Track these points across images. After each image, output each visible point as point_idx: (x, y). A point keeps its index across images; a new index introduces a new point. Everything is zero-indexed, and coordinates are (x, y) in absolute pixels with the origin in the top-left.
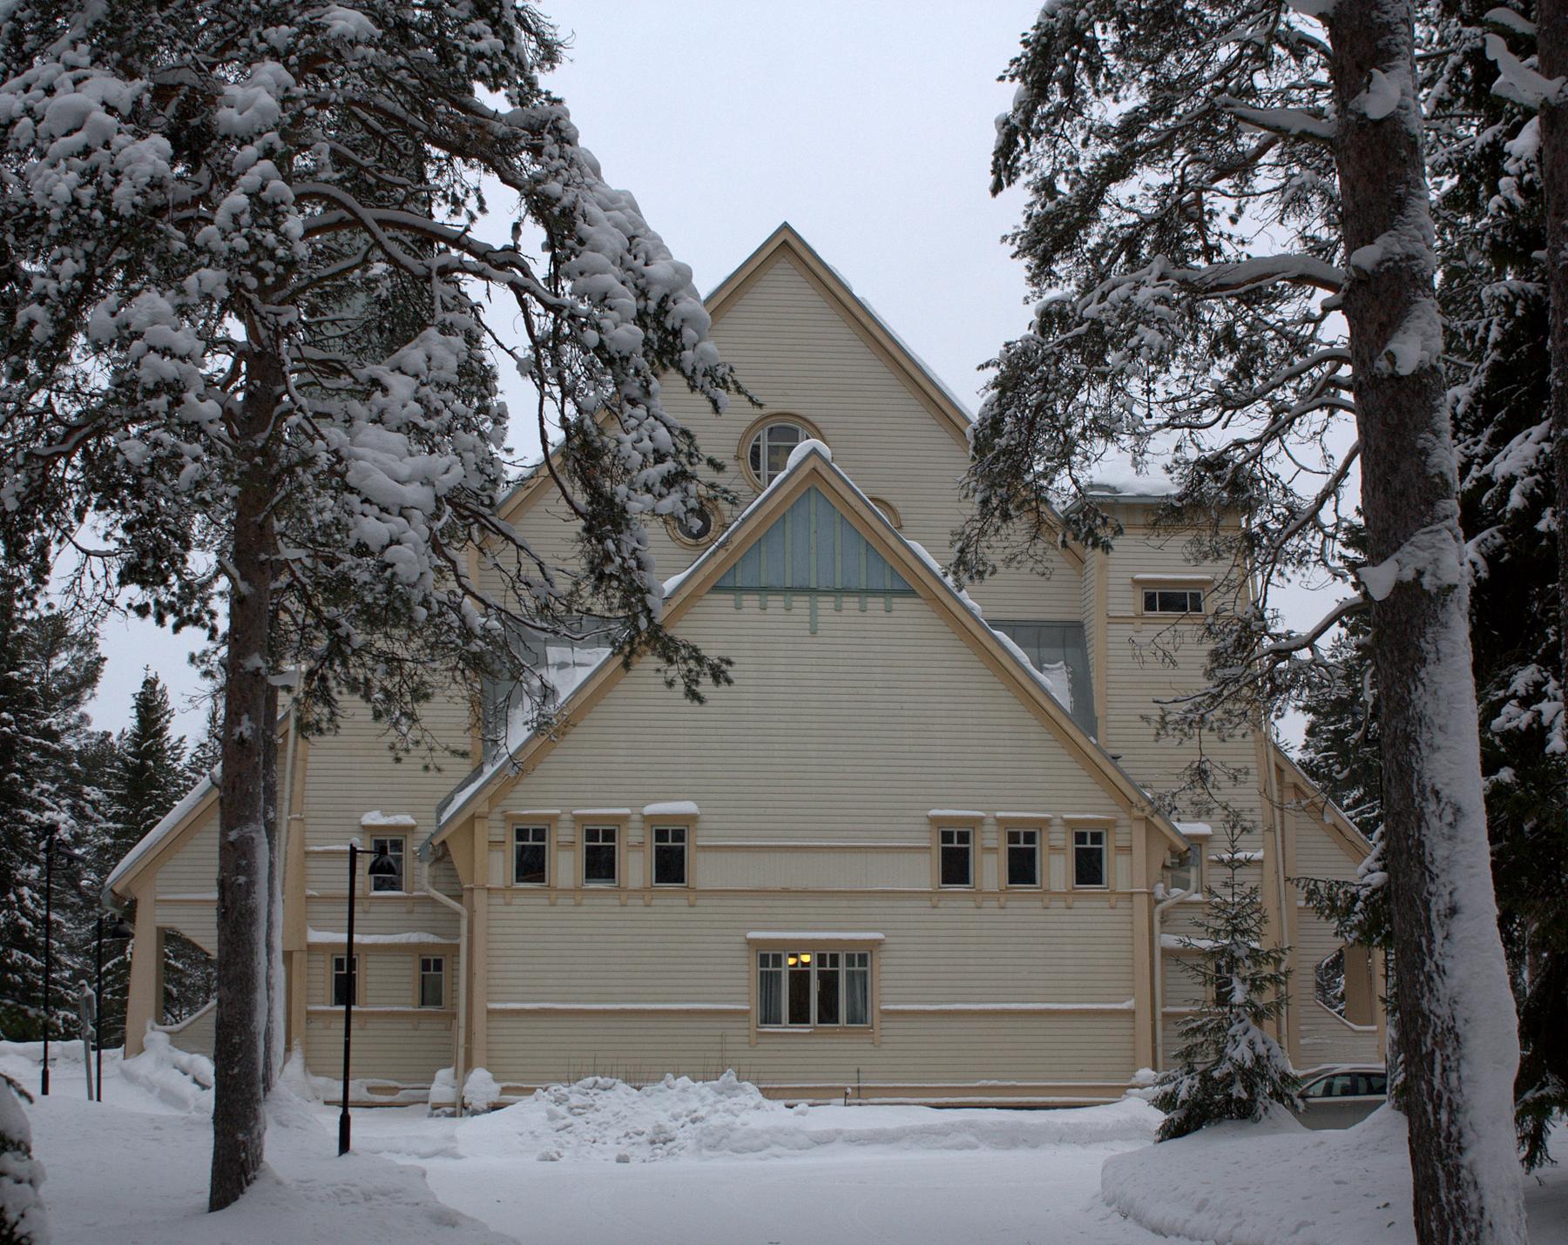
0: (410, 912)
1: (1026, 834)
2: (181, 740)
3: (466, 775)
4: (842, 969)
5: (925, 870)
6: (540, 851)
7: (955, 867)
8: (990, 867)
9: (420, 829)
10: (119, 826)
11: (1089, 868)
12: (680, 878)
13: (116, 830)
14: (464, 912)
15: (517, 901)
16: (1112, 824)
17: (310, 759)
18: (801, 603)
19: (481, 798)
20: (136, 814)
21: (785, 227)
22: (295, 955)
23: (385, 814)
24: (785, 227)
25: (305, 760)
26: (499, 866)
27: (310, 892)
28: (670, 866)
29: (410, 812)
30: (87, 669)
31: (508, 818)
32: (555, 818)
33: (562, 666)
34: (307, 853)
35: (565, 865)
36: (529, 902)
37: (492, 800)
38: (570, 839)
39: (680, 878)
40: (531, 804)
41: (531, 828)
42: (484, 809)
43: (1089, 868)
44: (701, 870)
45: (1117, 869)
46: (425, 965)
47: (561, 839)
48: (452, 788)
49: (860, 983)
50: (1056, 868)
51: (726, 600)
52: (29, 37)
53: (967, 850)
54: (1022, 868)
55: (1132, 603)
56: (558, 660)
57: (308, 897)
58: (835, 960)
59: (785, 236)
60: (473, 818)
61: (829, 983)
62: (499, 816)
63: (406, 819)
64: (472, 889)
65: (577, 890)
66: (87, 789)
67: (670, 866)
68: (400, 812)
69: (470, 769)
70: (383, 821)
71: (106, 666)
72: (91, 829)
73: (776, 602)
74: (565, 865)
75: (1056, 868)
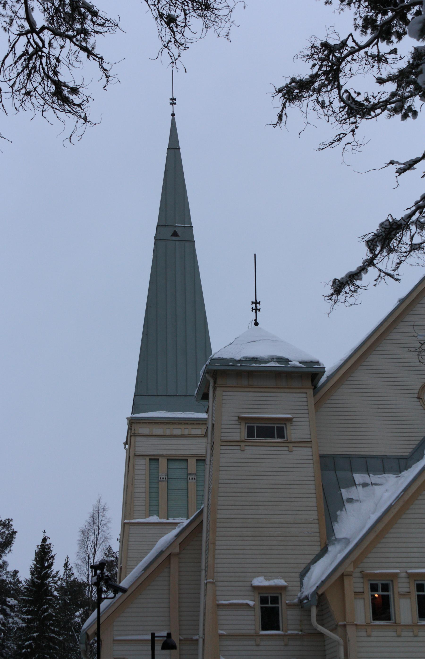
0: (286, 645)
2: (57, 573)
3: (317, 552)
9: (290, 588)
10: (29, 617)
13: (28, 619)
14: (342, 642)
15: (374, 634)
17: (217, 543)
19: (348, 561)
20: (38, 610)
23: (267, 578)
25: (214, 544)
27: (221, 632)
29: (283, 577)
30: (7, 537)
31: (364, 576)
32: (396, 575)
33: (365, 485)
34: (219, 606)
37: (356, 563)
38: (407, 590)
41: (279, 605)
42: (351, 569)
47: (401, 590)
48: (308, 561)
52: (66, 10)
56: (362, 482)
57: (221, 635)
60: (342, 576)
62: (359, 575)
63: (281, 582)
64: (345, 626)
65: (415, 625)
66: (8, 599)
68: (276, 577)
69: (319, 548)
70: (266, 583)
71: (17, 536)
72: (11, 620)
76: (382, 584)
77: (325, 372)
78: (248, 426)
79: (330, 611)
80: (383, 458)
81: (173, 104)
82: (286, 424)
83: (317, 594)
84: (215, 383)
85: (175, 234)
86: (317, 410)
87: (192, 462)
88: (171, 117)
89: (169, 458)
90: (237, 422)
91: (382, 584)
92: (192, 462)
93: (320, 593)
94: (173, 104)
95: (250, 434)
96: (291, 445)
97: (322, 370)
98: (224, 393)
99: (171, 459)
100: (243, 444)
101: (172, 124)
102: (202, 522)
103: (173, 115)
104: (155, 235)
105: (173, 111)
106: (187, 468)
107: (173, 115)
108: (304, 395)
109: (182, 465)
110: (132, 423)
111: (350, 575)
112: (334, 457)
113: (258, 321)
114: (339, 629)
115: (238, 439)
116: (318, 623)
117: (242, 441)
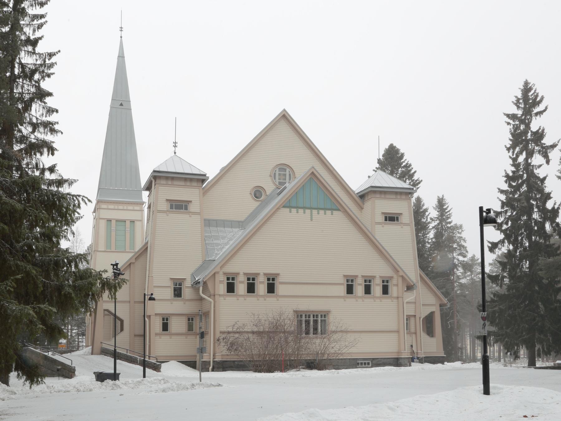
0: (184, 304)
1: (369, 280)
4: (319, 319)
5: (343, 290)
6: (352, 285)
7: (350, 290)
8: (359, 290)
11: (385, 290)
12: (253, 292)
16: (392, 278)
18: (308, 211)
21: (284, 110)
22: (151, 317)
24: (284, 110)
26: (222, 288)
28: (271, 289)
35: (241, 288)
36: (231, 299)
37: (221, 267)
39: (253, 292)
40: (231, 268)
43: (385, 290)
44: (280, 289)
45: (393, 290)
46: (189, 320)
49: (323, 322)
50: (377, 290)
51: (287, 210)
53: (274, 283)
54: (251, 288)
55: (381, 219)
58: (301, 316)
59: (284, 113)
60: (215, 274)
61: (316, 322)
67: (271, 289)
73: (301, 211)
74: (241, 288)
75: (377, 290)
76: (232, 278)
77: (209, 179)
78: (170, 204)
79: (207, 288)
80: (231, 221)
81: (121, 30)
82: (188, 203)
83: (203, 281)
84: (155, 182)
85: (121, 105)
86: (203, 196)
87: (128, 223)
88: (120, 38)
89: (116, 220)
90: (165, 202)
91: (232, 278)
92: (128, 223)
93: (204, 281)
94: (121, 30)
95: (171, 207)
96: (190, 214)
97: (208, 178)
98: (160, 187)
99: (117, 221)
100: (168, 212)
101: (120, 42)
102: (147, 247)
103: (121, 37)
104: (110, 104)
105: (121, 35)
106: (125, 225)
107: (121, 37)
108: (198, 190)
109: (123, 223)
110: (98, 202)
111: (218, 273)
112: (209, 220)
113: (176, 151)
114: (212, 297)
115: (166, 210)
116: (24, 305)
117: (167, 211)
